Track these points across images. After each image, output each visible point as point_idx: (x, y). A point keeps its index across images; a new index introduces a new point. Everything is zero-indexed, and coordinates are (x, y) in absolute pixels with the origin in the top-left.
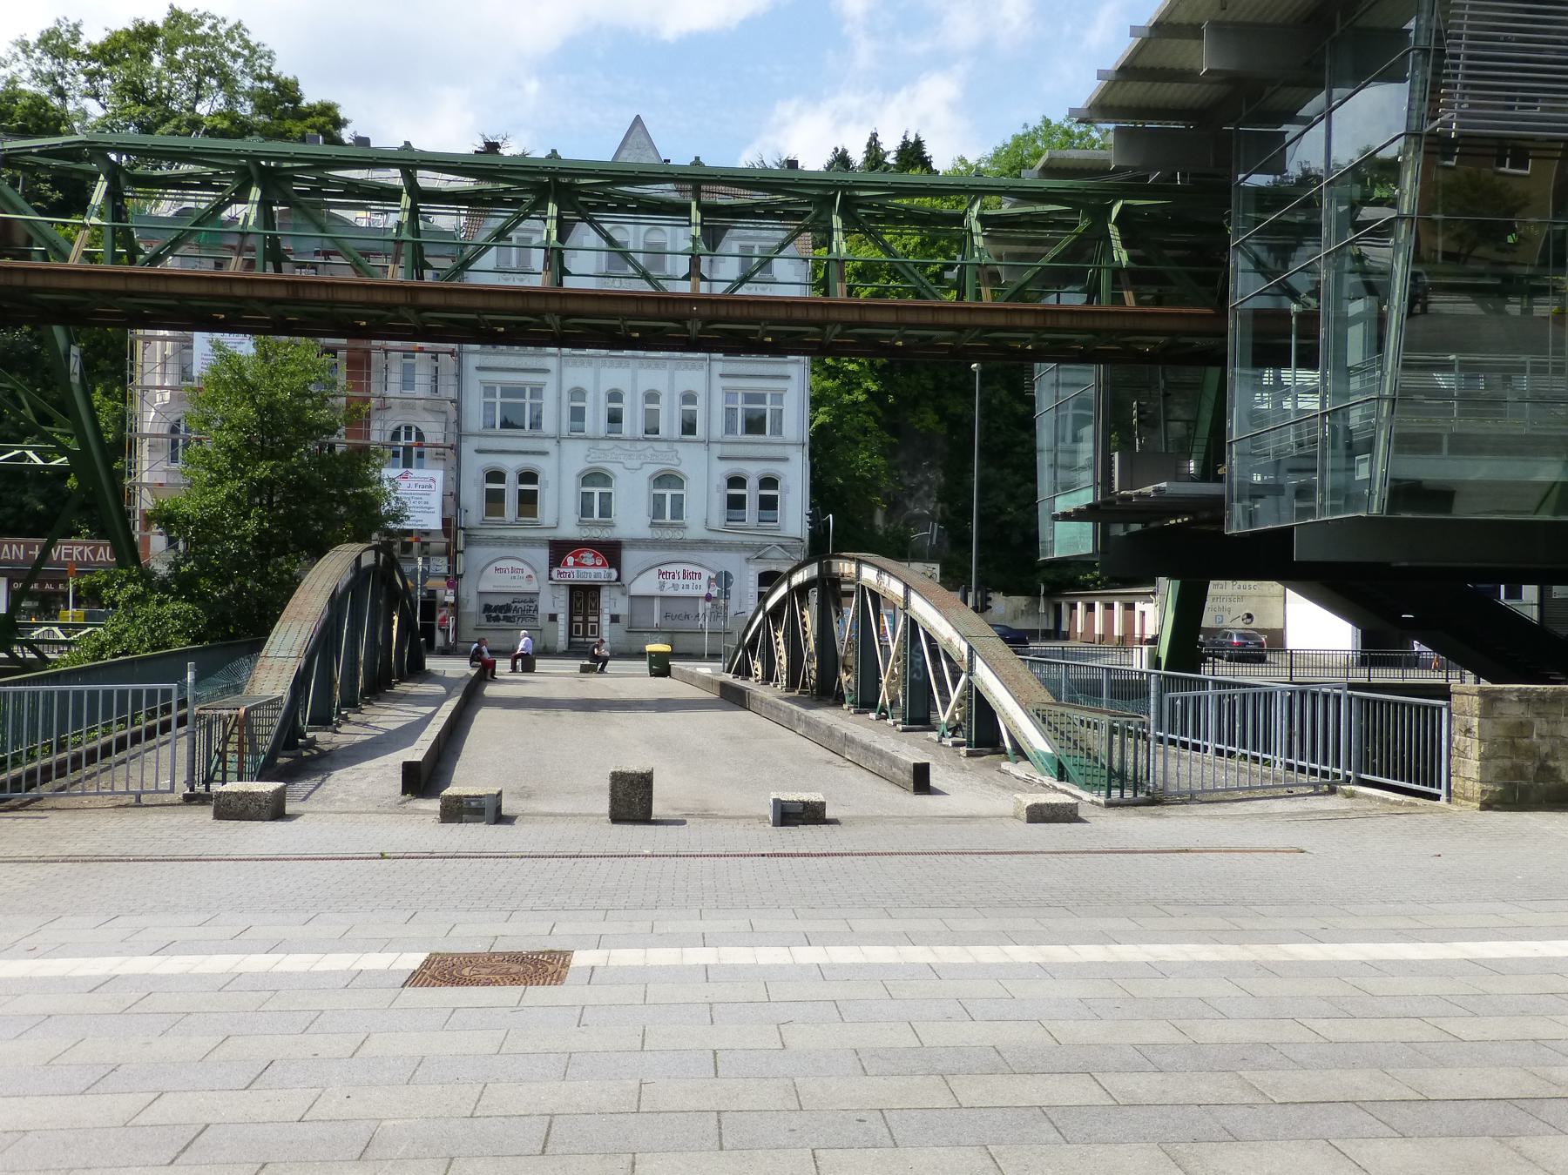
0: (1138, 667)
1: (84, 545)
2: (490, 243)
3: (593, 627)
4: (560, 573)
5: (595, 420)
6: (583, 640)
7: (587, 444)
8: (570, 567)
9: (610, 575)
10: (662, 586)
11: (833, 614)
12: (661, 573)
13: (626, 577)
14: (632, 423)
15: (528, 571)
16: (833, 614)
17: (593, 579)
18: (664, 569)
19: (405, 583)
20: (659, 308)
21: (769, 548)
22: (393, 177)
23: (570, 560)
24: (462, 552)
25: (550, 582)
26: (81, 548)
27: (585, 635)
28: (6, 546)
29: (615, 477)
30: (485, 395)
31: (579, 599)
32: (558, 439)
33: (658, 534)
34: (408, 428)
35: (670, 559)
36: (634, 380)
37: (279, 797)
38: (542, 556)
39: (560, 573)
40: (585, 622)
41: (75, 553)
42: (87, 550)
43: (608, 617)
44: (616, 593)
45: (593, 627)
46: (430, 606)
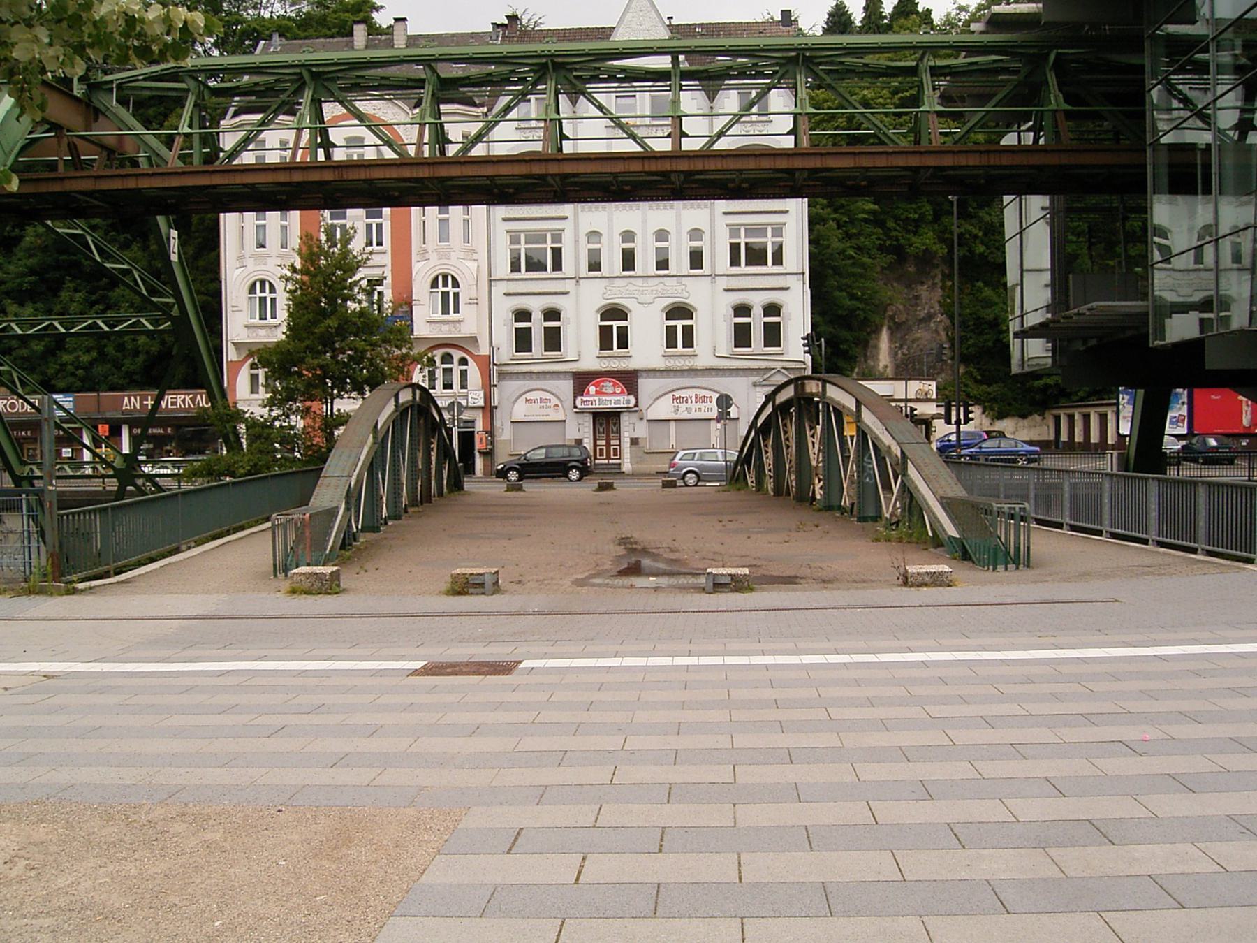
0: (1109, 470)
1: (185, 394)
2: (498, 119)
3: (615, 450)
4: (583, 402)
5: (612, 262)
6: (606, 461)
7: (605, 282)
8: (593, 396)
9: (628, 402)
10: (676, 411)
11: (807, 428)
12: (675, 398)
13: (643, 404)
14: (645, 262)
15: (554, 401)
16: (807, 428)
17: (613, 405)
18: (677, 394)
19: (440, 415)
20: (643, 165)
21: (774, 371)
22: (419, 71)
23: (592, 389)
24: (496, 386)
25: (575, 410)
26: (183, 397)
27: (608, 458)
28: (126, 398)
29: (630, 311)
30: (512, 243)
31: (601, 425)
32: (577, 279)
33: (671, 363)
34: (445, 277)
35: (688, 385)
36: (644, 221)
37: (335, 576)
38: (567, 386)
39: (583, 402)
40: (608, 445)
41: (179, 401)
42: (188, 399)
43: (628, 440)
44: (634, 417)
45: (615, 450)
46: (467, 439)
